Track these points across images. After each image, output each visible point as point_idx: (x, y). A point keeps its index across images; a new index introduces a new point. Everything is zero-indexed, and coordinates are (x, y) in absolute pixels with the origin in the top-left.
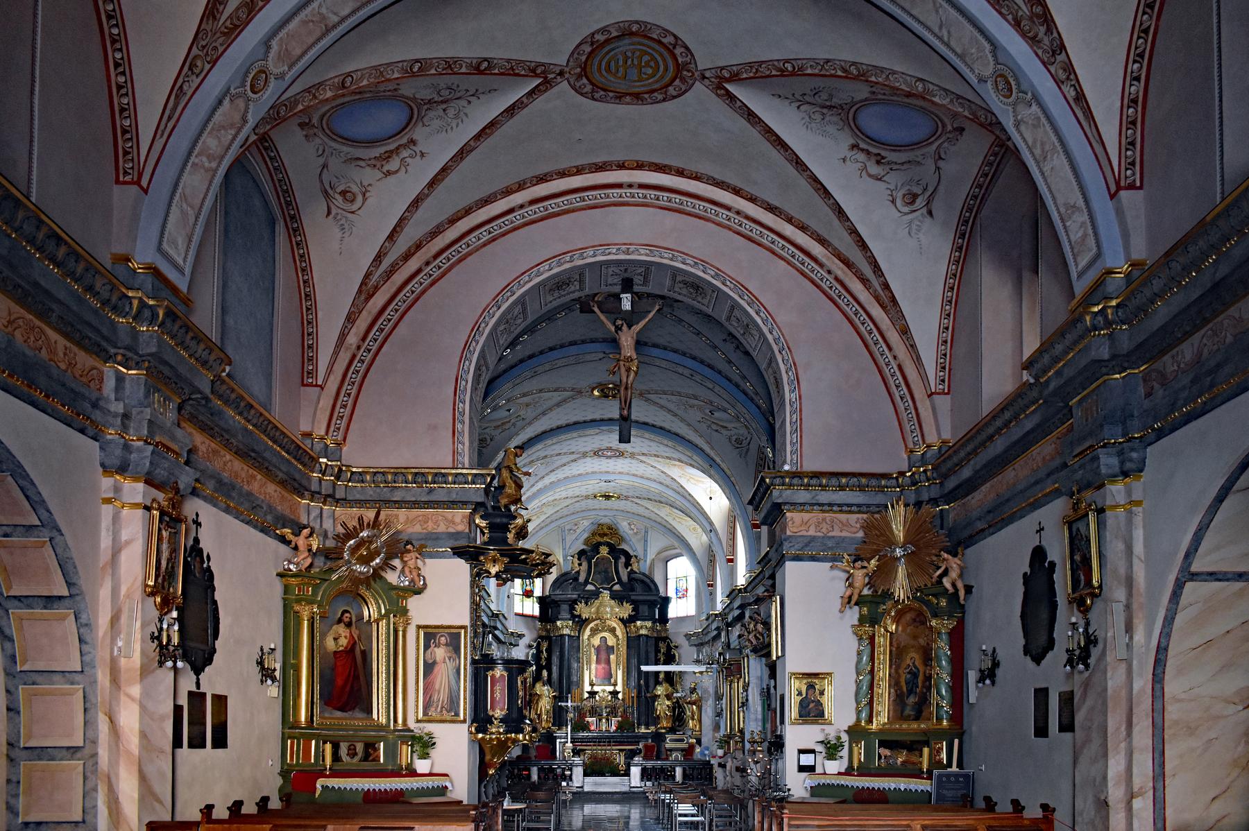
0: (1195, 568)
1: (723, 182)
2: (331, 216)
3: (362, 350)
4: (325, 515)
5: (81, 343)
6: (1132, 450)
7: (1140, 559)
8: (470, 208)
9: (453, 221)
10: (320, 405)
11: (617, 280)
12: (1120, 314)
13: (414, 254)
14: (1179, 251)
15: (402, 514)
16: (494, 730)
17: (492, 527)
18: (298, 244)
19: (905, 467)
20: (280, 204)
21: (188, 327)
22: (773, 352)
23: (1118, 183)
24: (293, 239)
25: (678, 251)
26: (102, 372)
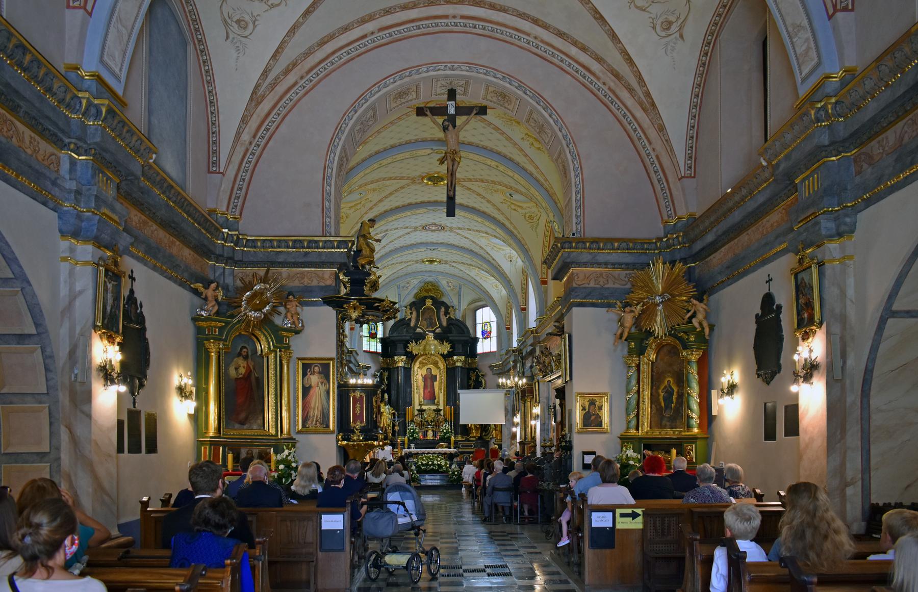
0: (895, 307)
1: (525, 14)
2: (229, 40)
3: (253, 145)
4: (227, 273)
5: (43, 133)
6: (847, 215)
7: (852, 301)
8: (334, 34)
9: (322, 43)
10: (222, 188)
11: (445, 91)
12: (838, 109)
13: (291, 70)
14: (889, 56)
15: (284, 271)
16: (355, 438)
17: (353, 282)
18: (204, 62)
19: (662, 234)
20: (191, 30)
21: (123, 123)
22: (562, 146)
23: (834, 6)
24: (201, 58)
25: (490, 68)
26: (58, 160)
